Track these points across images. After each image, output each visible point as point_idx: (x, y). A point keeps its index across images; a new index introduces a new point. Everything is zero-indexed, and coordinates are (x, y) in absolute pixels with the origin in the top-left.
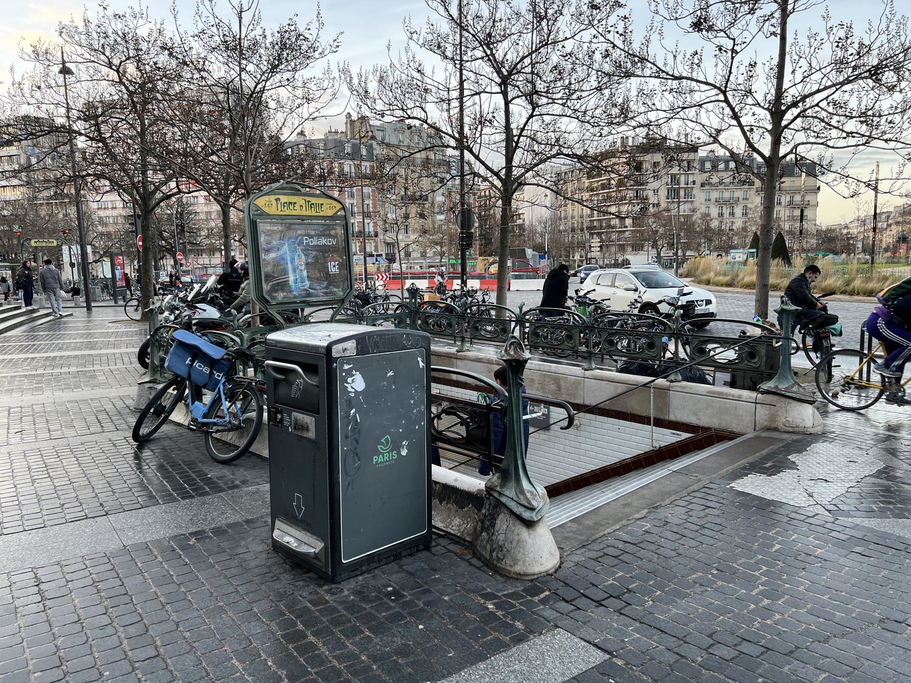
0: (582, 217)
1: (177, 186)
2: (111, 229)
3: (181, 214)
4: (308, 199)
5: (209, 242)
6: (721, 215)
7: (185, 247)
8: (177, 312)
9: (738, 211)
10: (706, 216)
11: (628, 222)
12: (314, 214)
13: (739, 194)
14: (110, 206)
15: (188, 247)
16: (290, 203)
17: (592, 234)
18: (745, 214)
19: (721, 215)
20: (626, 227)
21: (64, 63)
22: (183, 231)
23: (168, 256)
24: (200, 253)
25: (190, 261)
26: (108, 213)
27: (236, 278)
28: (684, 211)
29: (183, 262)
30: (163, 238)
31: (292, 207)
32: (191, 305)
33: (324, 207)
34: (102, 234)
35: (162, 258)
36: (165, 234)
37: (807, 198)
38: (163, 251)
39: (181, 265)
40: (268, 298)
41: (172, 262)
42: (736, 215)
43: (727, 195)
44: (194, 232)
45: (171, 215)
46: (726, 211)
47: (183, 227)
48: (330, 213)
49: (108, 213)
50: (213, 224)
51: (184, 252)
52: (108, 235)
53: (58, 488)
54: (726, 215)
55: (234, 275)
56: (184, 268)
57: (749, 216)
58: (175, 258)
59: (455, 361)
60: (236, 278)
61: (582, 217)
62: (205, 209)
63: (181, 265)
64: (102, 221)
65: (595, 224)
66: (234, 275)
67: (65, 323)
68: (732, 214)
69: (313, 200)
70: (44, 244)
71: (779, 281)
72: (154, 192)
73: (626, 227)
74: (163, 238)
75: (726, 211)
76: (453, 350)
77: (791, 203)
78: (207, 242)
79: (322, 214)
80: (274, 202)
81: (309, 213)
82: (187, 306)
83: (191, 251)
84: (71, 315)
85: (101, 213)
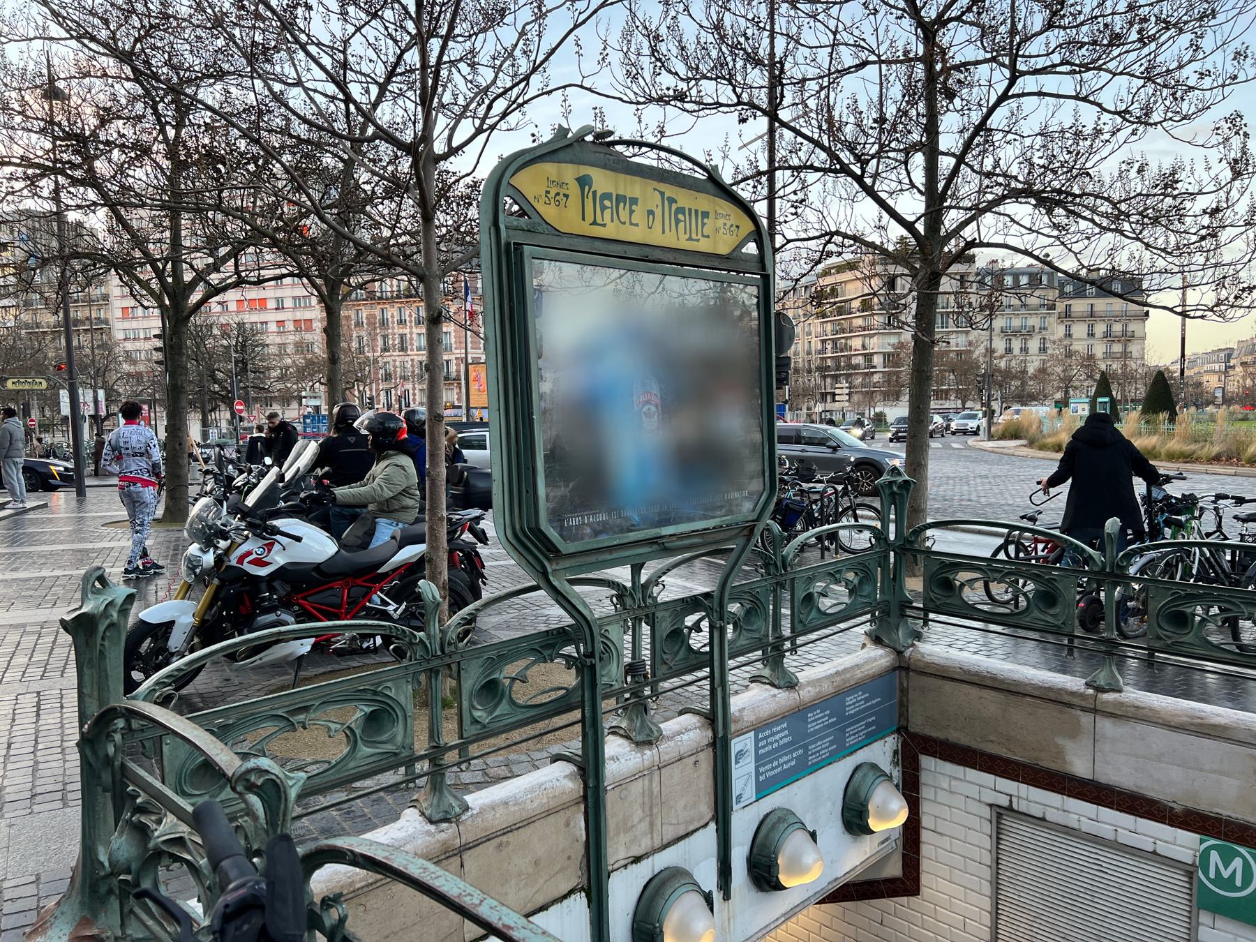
0: (809, 353)
1: (237, 272)
2: (141, 368)
3: (243, 346)
4: (670, 191)
5: (282, 386)
6: (1009, 350)
7: (247, 393)
8: (223, 544)
9: (1034, 345)
10: (990, 351)
11: (878, 360)
13: (1033, 321)
14: (142, 336)
15: (252, 394)
16: (620, 199)
17: (824, 377)
18: (1043, 349)
19: (1009, 350)
20: (874, 367)
21: (52, 80)
22: (244, 370)
23: (223, 407)
24: (268, 401)
25: (255, 413)
26: (139, 345)
27: (356, 445)
28: (957, 345)
29: (244, 414)
30: (216, 381)
32: (259, 523)
34: (129, 375)
35: (213, 410)
36: (220, 375)
37: (1131, 327)
38: (216, 399)
39: (241, 419)
40: (553, 534)
41: (228, 415)
42: (1030, 352)
43: (1016, 323)
44: (261, 372)
45: (227, 348)
46: (1016, 345)
47: (245, 364)
49: (139, 345)
50: (289, 361)
51: (247, 401)
52: (138, 376)
53: (41, 766)
54: (1016, 351)
55: (352, 439)
56: (245, 424)
57: (1050, 352)
58: (231, 409)
59: (1086, 719)
60: (356, 445)
61: (809, 353)
62: (278, 340)
63: (241, 419)
64: (129, 357)
65: (829, 362)
66: (352, 439)
67: (34, 522)
68: (1025, 350)
70: (27, 387)
71: (1193, 447)
72: (192, 285)
73: (874, 367)
74: (216, 381)
75: (1016, 345)
76: (1072, 683)
77: (1108, 334)
78: (280, 386)
80: (574, 189)
82: (250, 526)
83: (256, 400)
84: (45, 506)
85: (129, 346)
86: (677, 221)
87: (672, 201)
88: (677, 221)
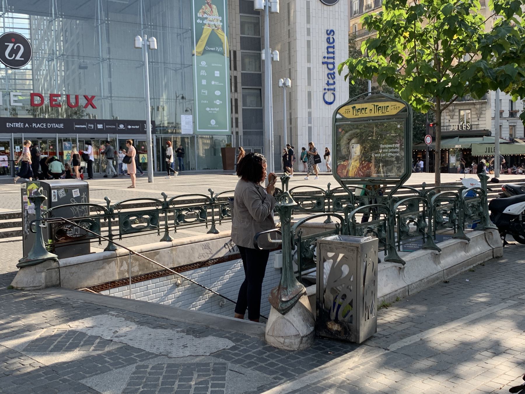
12: (381, 114)
31: (363, 111)
33: (389, 109)
48: (394, 112)
69: (381, 104)
79: (387, 114)
81: (377, 114)
86: (379, 110)
87: (377, 106)
88: (379, 110)
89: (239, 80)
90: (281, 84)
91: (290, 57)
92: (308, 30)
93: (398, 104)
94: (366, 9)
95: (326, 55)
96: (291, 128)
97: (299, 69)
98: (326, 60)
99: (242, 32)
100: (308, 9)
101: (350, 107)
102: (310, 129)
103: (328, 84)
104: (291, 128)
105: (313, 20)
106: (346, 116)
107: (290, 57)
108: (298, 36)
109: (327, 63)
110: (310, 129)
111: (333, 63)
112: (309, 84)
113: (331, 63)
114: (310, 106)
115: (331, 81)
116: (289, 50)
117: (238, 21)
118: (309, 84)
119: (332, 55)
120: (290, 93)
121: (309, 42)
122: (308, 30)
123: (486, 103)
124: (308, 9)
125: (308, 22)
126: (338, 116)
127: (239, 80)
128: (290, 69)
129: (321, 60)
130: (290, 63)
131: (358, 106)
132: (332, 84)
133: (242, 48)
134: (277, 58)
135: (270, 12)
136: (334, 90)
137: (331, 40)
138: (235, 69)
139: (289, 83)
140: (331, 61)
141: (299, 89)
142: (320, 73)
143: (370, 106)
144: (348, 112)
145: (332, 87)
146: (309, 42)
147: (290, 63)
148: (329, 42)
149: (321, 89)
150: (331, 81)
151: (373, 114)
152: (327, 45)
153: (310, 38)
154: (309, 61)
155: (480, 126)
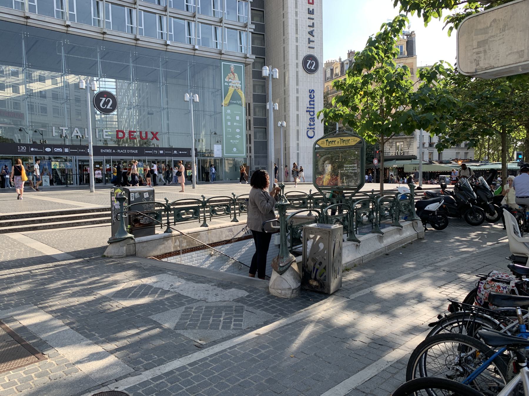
4: (342, 138)
12: (345, 145)
31: (333, 143)
33: (336, 143)
48: (354, 144)
69: (345, 138)
79: (349, 144)
81: (342, 145)
89: (252, 122)
90: (279, 125)
91: (284, 57)
92: (297, 90)
93: (356, 138)
94: (335, 76)
95: (309, 106)
96: (285, 154)
97: (291, 115)
98: (309, 109)
99: (254, 91)
100: (297, 76)
101: (325, 140)
102: (298, 154)
103: (310, 125)
104: (285, 154)
105: (300, 83)
106: (322, 146)
107: (284, 57)
108: (291, 94)
109: (310, 111)
110: (298, 154)
111: (314, 112)
112: (298, 125)
113: (312, 111)
114: (298, 139)
115: (312, 123)
116: (285, 102)
117: (252, 84)
118: (298, 125)
119: (312, 106)
120: (285, 131)
121: (297, 98)
122: (297, 90)
123: (413, 138)
124: (297, 76)
125: (297, 84)
126: (317, 146)
127: (252, 122)
128: (285, 115)
129: (306, 109)
130: (285, 111)
131: (330, 140)
132: (312, 125)
133: (254, 101)
134: (277, 108)
135: (272, 78)
136: (314, 129)
137: (312, 96)
138: (249, 115)
139: (285, 124)
140: (312, 110)
141: (291, 127)
142: (305, 118)
143: (337, 139)
144: (323, 143)
145: (312, 127)
146: (297, 98)
147: (285, 111)
148: (311, 98)
149: (306, 128)
150: (312, 123)
151: (339, 145)
152: (309, 99)
153: (299, 95)
154: (298, 110)
155: (410, 153)
